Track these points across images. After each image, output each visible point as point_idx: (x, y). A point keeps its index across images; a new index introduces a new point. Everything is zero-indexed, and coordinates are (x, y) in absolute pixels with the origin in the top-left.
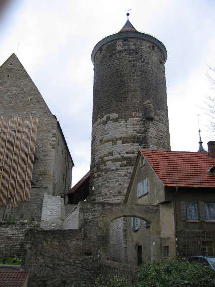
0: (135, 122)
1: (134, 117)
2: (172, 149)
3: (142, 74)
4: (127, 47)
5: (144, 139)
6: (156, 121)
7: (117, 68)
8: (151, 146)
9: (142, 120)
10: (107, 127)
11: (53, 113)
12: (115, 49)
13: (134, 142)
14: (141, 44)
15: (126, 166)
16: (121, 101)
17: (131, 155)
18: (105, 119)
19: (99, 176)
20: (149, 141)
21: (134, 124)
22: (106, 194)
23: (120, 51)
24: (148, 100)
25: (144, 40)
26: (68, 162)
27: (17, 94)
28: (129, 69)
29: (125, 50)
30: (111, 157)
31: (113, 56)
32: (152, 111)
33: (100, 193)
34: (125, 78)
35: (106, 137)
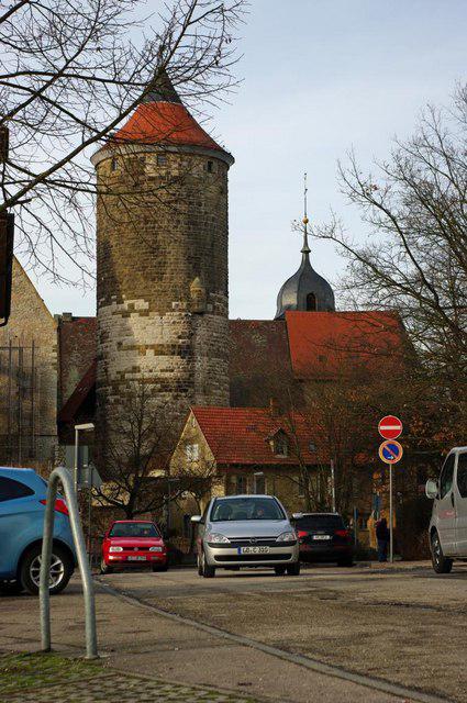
0: (175, 319)
1: (174, 310)
2: (232, 317)
13: (173, 354)
17: (167, 375)
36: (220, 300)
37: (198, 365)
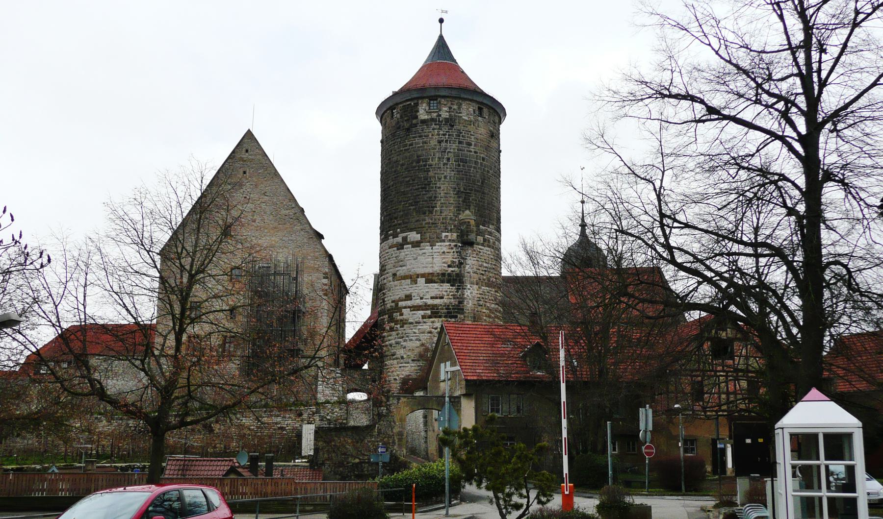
0: (445, 249)
1: (444, 241)
3: (459, 165)
4: (435, 114)
5: (457, 275)
6: (478, 244)
7: (419, 153)
8: (469, 286)
9: (456, 246)
10: (403, 253)
11: (315, 226)
12: (417, 117)
13: (443, 282)
14: (459, 108)
15: (430, 317)
16: (425, 213)
18: (399, 239)
19: (392, 329)
20: (466, 279)
21: (444, 252)
22: (402, 358)
23: (424, 122)
24: (467, 212)
25: (465, 99)
26: (339, 290)
27: (263, 205)
28: (438, 140)
29: (432, 120)
30: (409, 303)
31: (414, 129)
32: (472, 232)
33: (393, 355)
34: (431, 174)
35: (402, 271)
36: (490, 234)
37: (467, 293)
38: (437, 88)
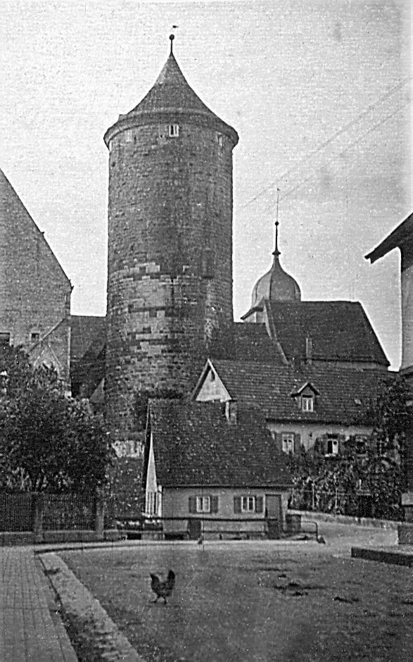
19: (128, 362)
28: (175, 146)
30: (147, 336)
35: (140, 303)
38: (14, 544)
